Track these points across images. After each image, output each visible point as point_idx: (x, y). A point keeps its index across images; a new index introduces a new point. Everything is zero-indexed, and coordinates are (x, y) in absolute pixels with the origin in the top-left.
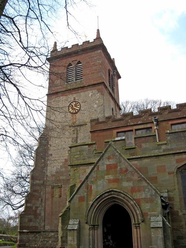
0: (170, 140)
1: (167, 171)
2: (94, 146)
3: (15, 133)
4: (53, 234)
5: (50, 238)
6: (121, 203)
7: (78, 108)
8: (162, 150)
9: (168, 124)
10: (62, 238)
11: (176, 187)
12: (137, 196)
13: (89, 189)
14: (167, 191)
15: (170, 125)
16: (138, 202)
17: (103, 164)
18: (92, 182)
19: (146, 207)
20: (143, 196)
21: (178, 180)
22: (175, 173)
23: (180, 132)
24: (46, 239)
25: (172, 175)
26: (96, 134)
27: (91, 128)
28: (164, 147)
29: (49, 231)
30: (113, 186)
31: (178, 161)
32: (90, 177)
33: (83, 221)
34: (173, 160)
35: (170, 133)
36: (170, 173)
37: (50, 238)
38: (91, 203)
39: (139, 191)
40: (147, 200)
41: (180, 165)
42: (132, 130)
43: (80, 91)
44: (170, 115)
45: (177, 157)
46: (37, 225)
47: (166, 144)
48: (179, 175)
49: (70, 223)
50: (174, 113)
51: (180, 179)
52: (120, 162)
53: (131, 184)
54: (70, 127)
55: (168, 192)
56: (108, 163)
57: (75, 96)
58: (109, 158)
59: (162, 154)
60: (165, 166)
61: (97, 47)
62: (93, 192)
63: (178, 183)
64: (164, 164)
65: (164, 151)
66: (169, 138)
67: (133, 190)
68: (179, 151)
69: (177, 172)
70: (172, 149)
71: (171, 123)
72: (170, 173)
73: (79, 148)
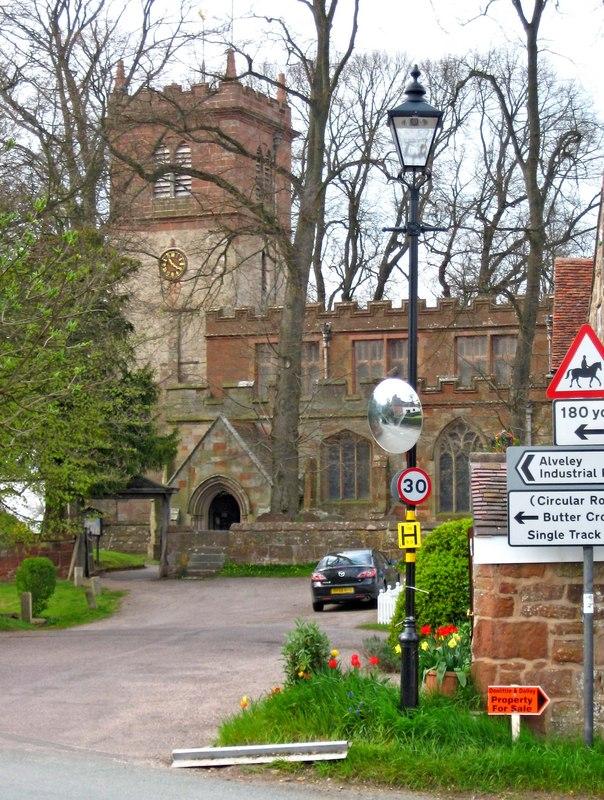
2: (206, 391)
4: (134, 529)
5: (128, 536)
6: (231, 492)
7: (180, 268)
9: (347, 339)
10: (156, 532)
12: (248, 483)
13: (191, 472)
15: (350, 342)
16: (247, 491)
17: (209, 441)
18: (196, 464)
19: (255, 497)
20: (253, 485)
24: (122, 538)
26: (216, 343)
27: (208, 330)
30: (220, 471)
32: (193, 457)
33: (185, 510)
37: (128, 536)
38: (194, 489)
39: (249, 478)
40: (256, 489)
43: (185, 224)
44: (353, 322)
49: (540, 117)
52: (230, 441)
53: (241, 470)
54: (165, 311)
56: (216, 441)
57: (173, 234)
58: (216, 435)
62: (197, 477)
67: (242, 477)
73: (181, 392)
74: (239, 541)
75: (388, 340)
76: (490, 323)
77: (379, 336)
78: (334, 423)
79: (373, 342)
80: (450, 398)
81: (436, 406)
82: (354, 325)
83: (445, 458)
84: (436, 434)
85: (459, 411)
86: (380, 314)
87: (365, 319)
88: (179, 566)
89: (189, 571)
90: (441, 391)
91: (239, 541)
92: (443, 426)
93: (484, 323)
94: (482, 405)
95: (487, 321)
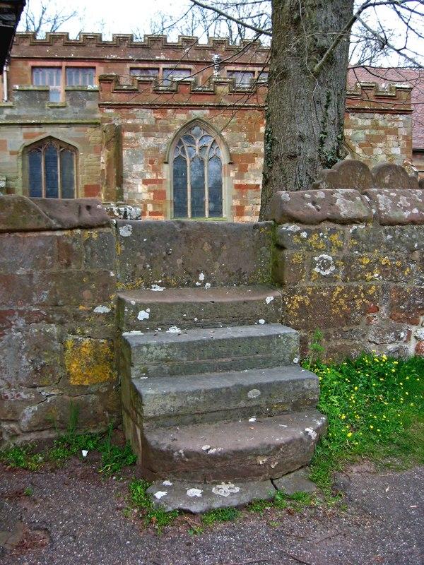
0: (18, 102)
1: (9, 149)
3: (66, 18)
8: (5, 116)
9: (26, 64)
11: (20, 174)
14: (5, 179)
21: (23, 164)
22: (20, 154)
23: (35, 91)
25: (15, 156)
28: (7, 112)
29: (332, 225)
31: (26, 136)
34: (19, 133)
35: (19, 90)
36: (12, 153)
41: (28, 142)
42: (158, 69)
44: (33, 49)
45: (25, 130)
46: (153, 115)
47: (11, 107)
48: (27, 158)
50: (40, 47)
51: (27, 163)
55: (7, 180)
59: (4, 122)
60: (5, 141)
61: (68, 33)
63: (23, 169)
64: (4, 139)
65: (8, 117)
66: (16, 98)
68: (28, 121)
69: (23, 151)
70: (19, 117)
71: (31, 63)
72: (12, 153)
74: (325, 264)
75: (67, 67)
76: (163, 58)
77: (57, 64)
78: (37, 130)
79: (51, 70)
80: (183, 99)
81: (170, 106)
82: (33, 52)
83: (180, 161)
84: (171, 135)
85: (197, 113)
86: (59, 44)
87: (44, 48)
88: (50, 393)
89: (162, 440)
90: (176, 92)
91: (325, 264)
92: (178, 127)
93: (157, 58)
94: (220, 107)
95: (160, 55)
